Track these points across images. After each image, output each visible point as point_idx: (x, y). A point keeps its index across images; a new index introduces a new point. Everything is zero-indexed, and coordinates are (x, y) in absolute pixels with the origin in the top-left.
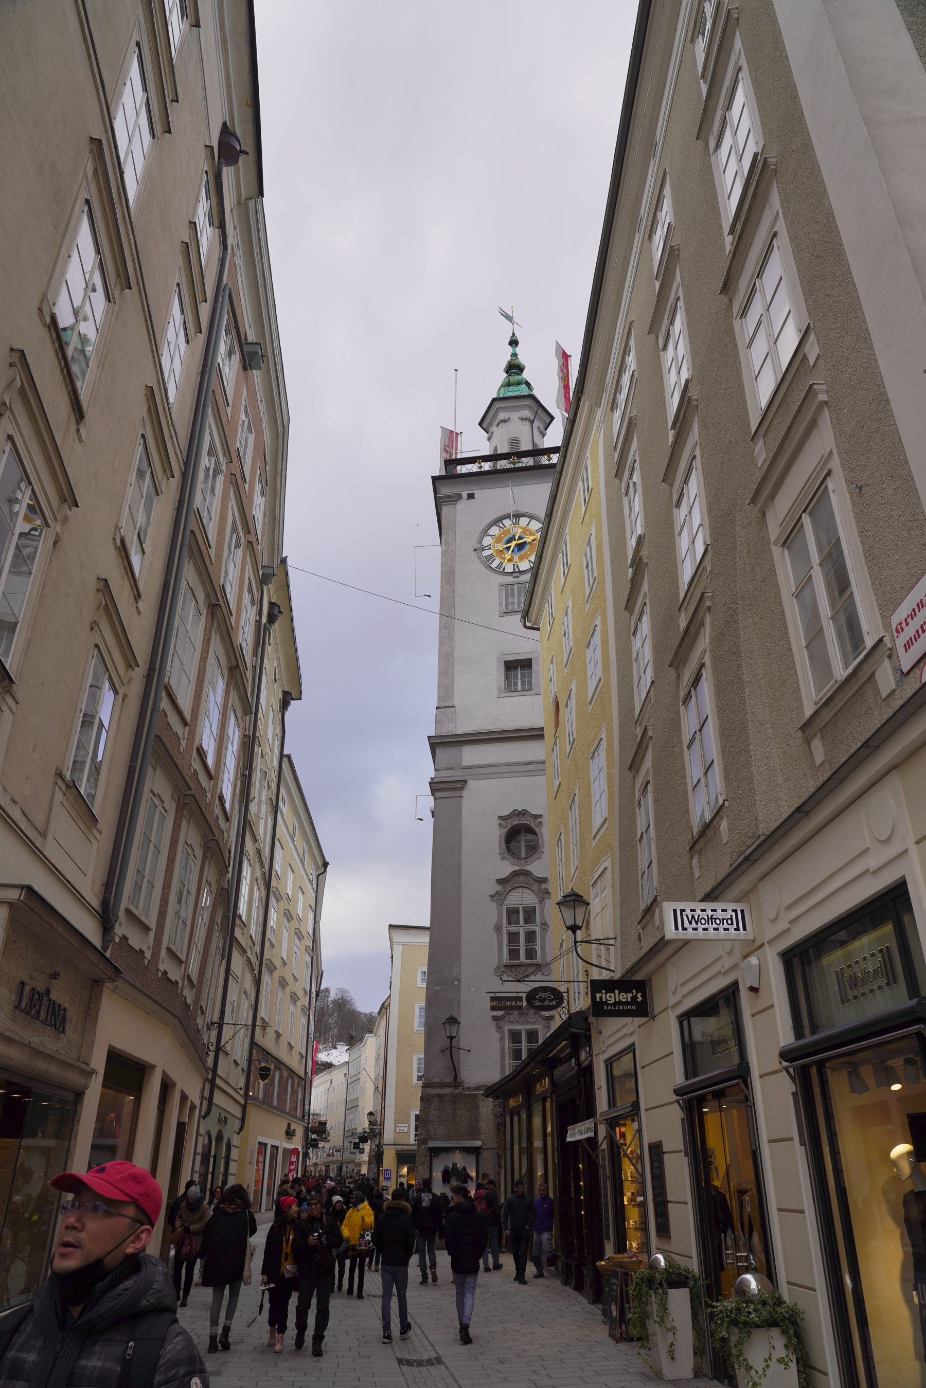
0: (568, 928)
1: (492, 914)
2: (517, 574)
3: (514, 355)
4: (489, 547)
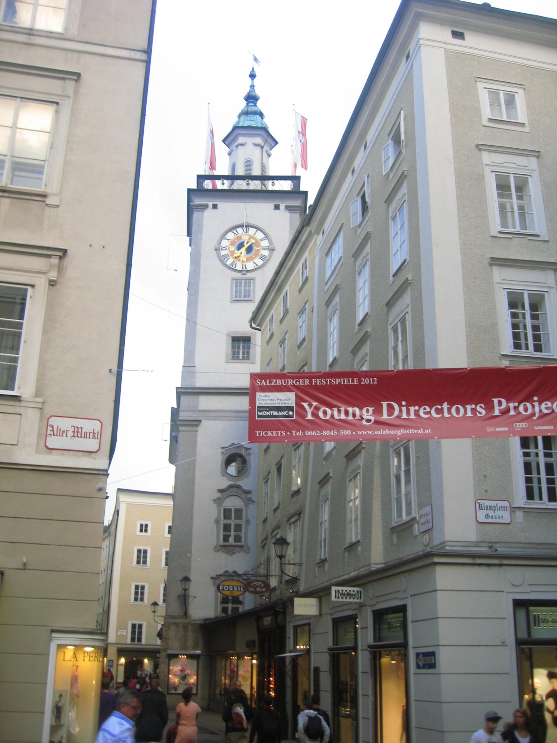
0: (278, 556)
1: (213, 512)
2: (245, 272)
3: (252, 86)
4: (226, 248)
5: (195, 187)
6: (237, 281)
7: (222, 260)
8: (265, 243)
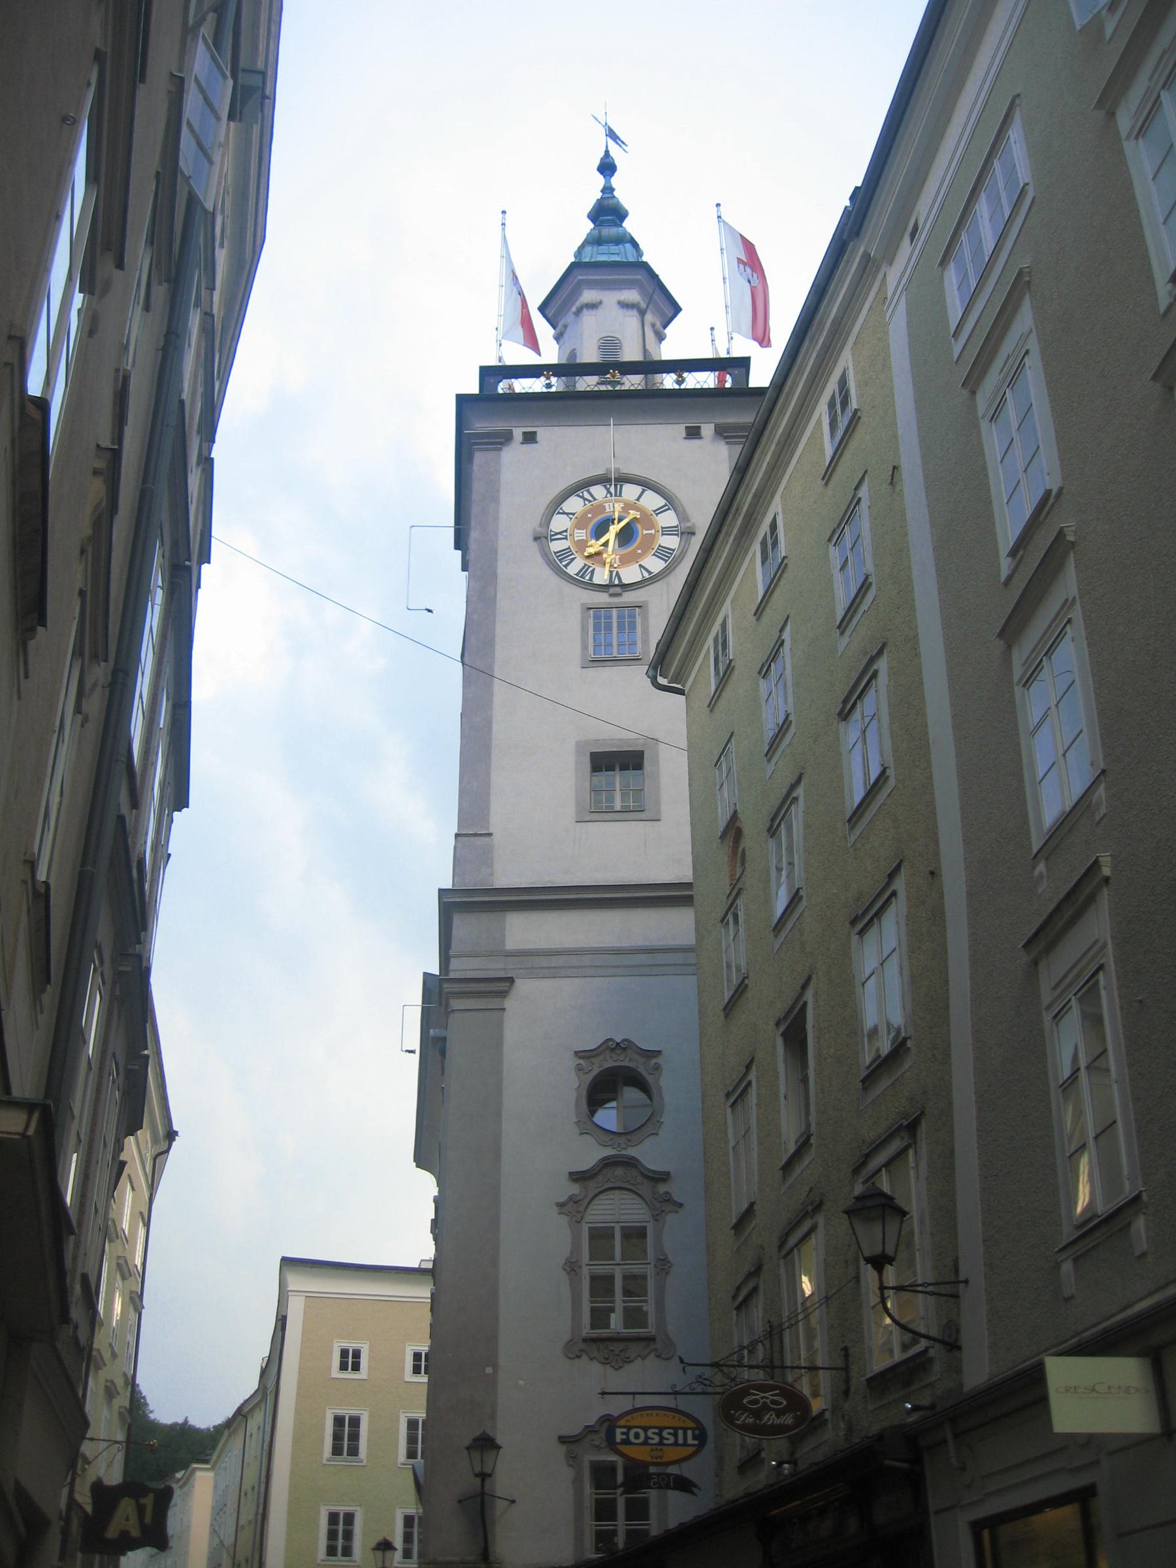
1: (559, 1237)
2: (618, 590)
3: (608, 190)
4: (563, 535)
5: (476, 391)
6: (598, 617)
7: (556, 562)
8: (669, 519)
